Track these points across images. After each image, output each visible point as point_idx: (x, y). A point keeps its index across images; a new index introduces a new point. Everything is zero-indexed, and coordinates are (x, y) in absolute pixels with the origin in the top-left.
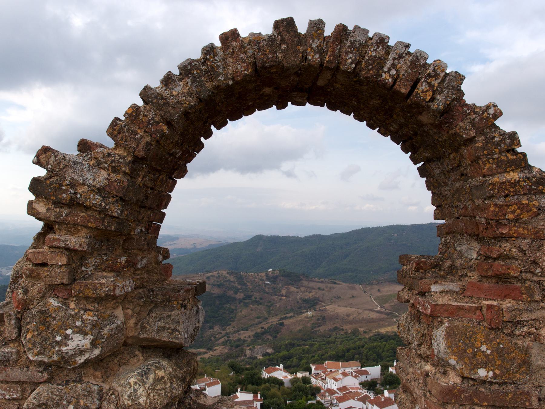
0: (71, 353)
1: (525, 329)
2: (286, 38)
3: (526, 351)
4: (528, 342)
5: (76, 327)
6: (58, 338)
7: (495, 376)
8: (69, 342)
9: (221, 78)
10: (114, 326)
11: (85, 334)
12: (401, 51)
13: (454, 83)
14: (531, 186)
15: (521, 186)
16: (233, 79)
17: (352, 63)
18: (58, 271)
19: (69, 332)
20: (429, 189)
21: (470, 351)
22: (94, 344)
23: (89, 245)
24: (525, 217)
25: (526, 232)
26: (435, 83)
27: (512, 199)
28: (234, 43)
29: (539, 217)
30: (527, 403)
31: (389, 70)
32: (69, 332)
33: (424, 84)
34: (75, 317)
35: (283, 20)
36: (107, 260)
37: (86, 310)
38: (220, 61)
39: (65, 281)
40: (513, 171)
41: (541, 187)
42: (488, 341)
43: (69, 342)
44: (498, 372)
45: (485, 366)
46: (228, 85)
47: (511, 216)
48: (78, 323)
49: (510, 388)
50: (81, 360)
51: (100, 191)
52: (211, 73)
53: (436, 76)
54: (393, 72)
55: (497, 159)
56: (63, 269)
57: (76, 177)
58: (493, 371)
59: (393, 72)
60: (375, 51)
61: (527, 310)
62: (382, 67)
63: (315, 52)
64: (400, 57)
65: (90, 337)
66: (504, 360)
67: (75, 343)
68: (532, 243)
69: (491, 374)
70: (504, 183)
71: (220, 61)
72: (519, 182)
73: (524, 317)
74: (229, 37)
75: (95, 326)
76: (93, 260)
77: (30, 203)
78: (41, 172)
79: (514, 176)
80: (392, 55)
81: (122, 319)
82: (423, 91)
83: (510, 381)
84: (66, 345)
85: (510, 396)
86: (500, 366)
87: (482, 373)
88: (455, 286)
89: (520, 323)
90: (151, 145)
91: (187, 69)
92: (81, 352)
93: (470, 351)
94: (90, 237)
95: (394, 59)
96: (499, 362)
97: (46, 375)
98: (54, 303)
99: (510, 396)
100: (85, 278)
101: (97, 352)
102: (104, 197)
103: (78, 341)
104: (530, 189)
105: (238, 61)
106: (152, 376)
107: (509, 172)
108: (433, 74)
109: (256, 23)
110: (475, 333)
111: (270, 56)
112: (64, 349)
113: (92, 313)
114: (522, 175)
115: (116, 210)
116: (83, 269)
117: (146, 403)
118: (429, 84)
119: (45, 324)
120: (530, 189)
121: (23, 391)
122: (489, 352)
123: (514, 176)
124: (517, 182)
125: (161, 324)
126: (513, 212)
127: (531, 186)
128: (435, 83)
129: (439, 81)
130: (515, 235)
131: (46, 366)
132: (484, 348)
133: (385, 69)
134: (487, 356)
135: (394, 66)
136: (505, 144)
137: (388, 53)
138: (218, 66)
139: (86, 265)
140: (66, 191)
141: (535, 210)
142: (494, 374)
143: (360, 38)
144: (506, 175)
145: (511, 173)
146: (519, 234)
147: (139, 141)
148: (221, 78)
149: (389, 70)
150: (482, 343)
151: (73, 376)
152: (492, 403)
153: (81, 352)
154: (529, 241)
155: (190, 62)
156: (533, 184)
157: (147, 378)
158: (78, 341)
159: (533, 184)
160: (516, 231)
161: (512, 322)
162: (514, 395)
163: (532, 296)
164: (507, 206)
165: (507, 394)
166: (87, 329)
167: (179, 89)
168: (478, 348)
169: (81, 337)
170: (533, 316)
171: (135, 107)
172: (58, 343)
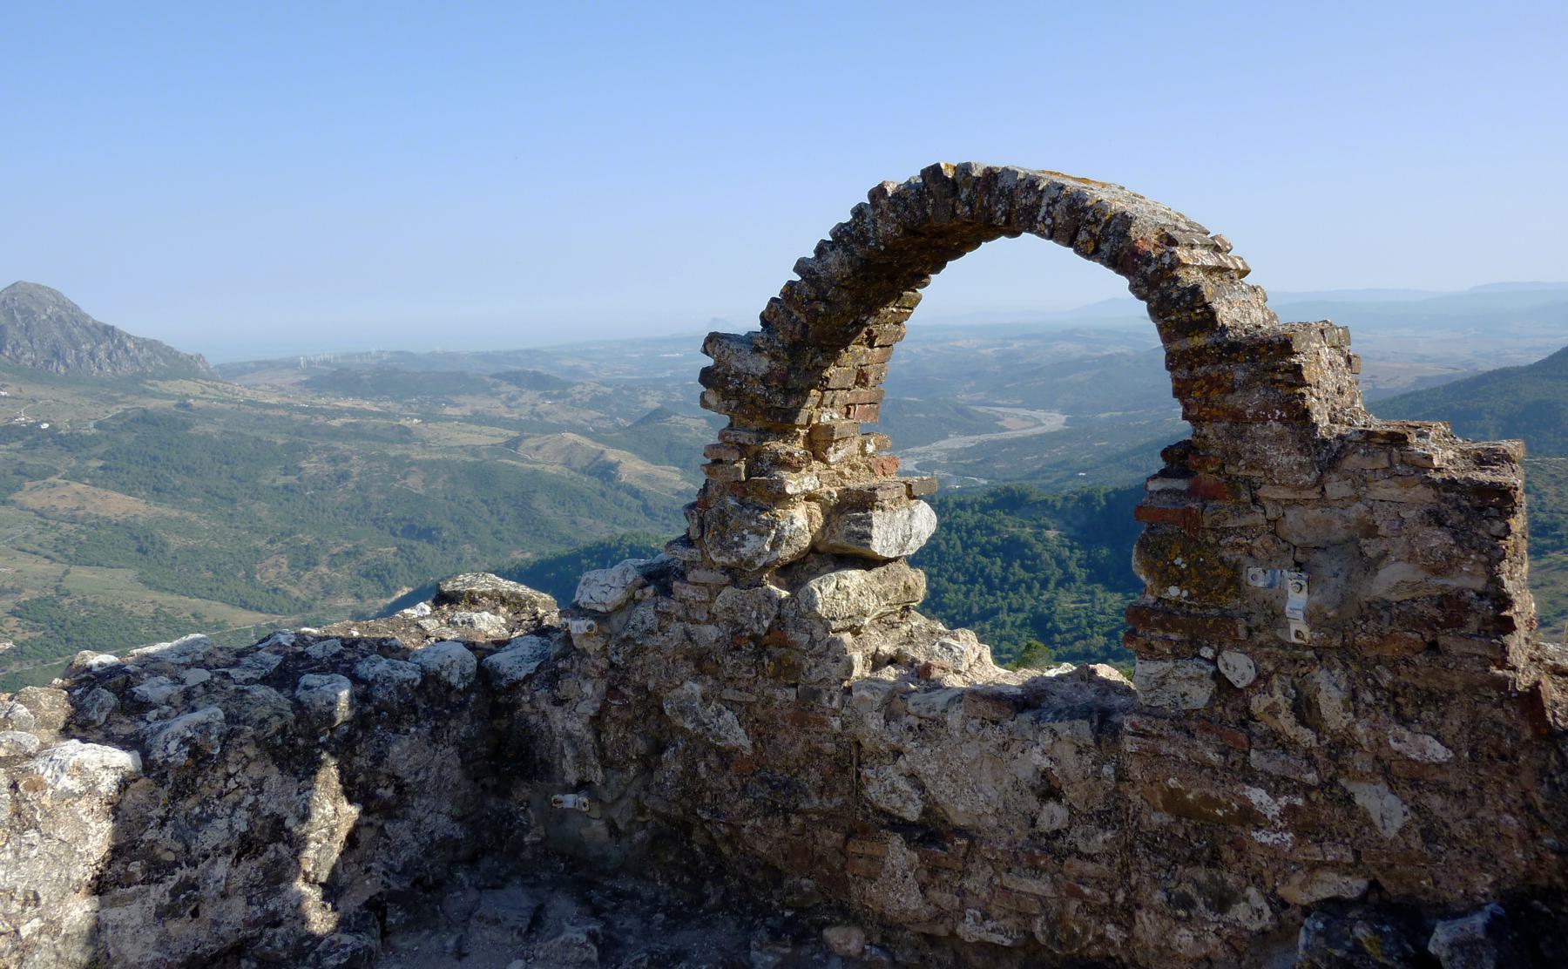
1: (1231, 539)
3: (1236, 567)
4: (1239, 554)
9: (872, 244)
12: (1055, 193)
13: (1120, 228)
26: (1097, 230)
27: (1199, 371)
45: (1178, 583)
52: (862, 239)
53: (1097, 222)
59: (1049, 221)
62: (1035, 218)
63: (965, 204)
64: (1055, 201)
69: (1185, 593)
70: (1186, 352)
73: (1230, 524)
74: (878, 193)
77: (703, 395)
78: (709, 362)
79: (1199, 341)
80: (1045, 201)
88: (19, 445)
89: (1226, 532)
91: (841, 233)
105: (887, 221)
109: (901, 172)
110: (1171, 543)
112: (742, 550)
118: (1090, 233)
123: (1199, 341)
128: (1097, 230)
131: (728, 570)
132: (1178, 561)
134: (1181, 572)
135: (1048, 213)
137: (1041, 198)
143: (1010, 183)
147: (794, 323)
148: (872, 244)
152: (789, 610)
154: (1226, 424)
155: (842, 225)
156: (1224, 350)
159: (1224, 350)
167: (832, 259)
170: (1242, 522)
171: (791, 284)
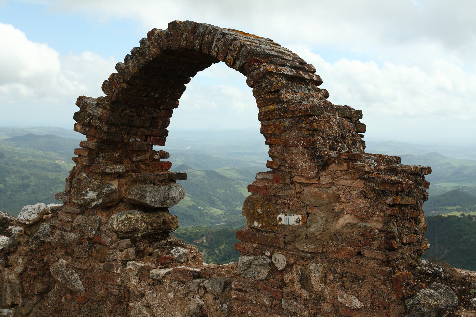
0: (89, 200)
2: (172, 33)
5: (91, 187)
6: (84, 192)
7: (262, 227)
8: (88, 195)
10: (110, 189)
11: (94, 191)
14: (280, 114)
15: (275, 114)
16: (152, 57)
17: (198, 46)
18: (85, 159)
19: (88, 189)
20: (259, 119)
21: (252, 211)
22: (99, 197)
23: (96, 146)
24: (277, 132)
25: (280, 141)
28: (152, 37)
29: (286, 133)
30: (278, 244)
31: (214, 48)
32: (88, 189)
33: (229, 55)
34: (90, 182)
35: (191, 23)
36: (108, 155)
37: (96, 179)
38: (147, 48)
39: (87, 164)
40: (272, 104)
41: (286, 114)
42: (262, 207)
43: (88, 195)
44: (264, 224)
45: (258, 220)
46: (150, 60)
47: (270, 132)
48: (91, 185)
49: (272, 235)
50: (93, 204)
51: (99, 119)
54: (216, 49)
55: (264, 97)
56: (87, 158)
57: (90, 112)
58: (262, 223)
60: (207, 38)
61: (282, 189)
65: (96, 193)
66: (269, 218)
67: (90, 195)
68: (283, 148)
69: (260, 225)
70: (266, 112)
71: (147, 48)
72: (274, 111)
75: (99, 187)
76: (102, 154)
81: (116, 186)
82: (229, 60)
83: (271, 231)
84: (87, 196)
85: (270, 239)
86: (267, 221)
87: (256, 224)
90: (119, 94)
92: (93, 200)
93: (252, 211)
94: (98, 142)
95: (216, 41)
96: (266, 219)
97: (79, 210)
98: (84, 175)
99: (270, 239)
100: (98, 163)
101: (100, 201)
102: (101, 122)
103: (91, 195)
104: (280, 115)
106: (124, 216)
107: (270, 105)
108: (233, 49)
110: (258, 202)
111: (166, 43)
113: (98, 181)
114: (277, 107)
115: (105, 128)
116: (98, 159)
117: (116, 228)
118: (232, 55)
119: (79, 185)
120: (280, 115)
121: (72, 218)
122: (261, 212)
124: (273, 111)
125: (137, 191)
126: (271, 129)
127: (280, 114)
129: (236, 53)
130: (274, 143)
131: (80, 206)
132: (259, 210)
133: (212, 48)
134: (260, 215)
135: (216, 45)
136: (267, 89)
138: (146, 51)
139: (99, 157)
140: (86, 118)
141: (282, 128)
142: (262, 225)
144: (268, 107)
145: (271, 106)
146: (276, 142)
148: (147, 57)
149: (214, 48)
150: (259, 208)
151: (92, 213)
153: (93, 200)
154: (281, 147)
157: (121, 217)
158: (91, 195)
160: (274, 141)
161: (275, 196)
162: (272, 239)
163: (284, 180)
164: (268, 125)
165: (268, 238)
166: (95, 188)
168: (256, 210)
169: (92, 193)
172: (83, 194)
